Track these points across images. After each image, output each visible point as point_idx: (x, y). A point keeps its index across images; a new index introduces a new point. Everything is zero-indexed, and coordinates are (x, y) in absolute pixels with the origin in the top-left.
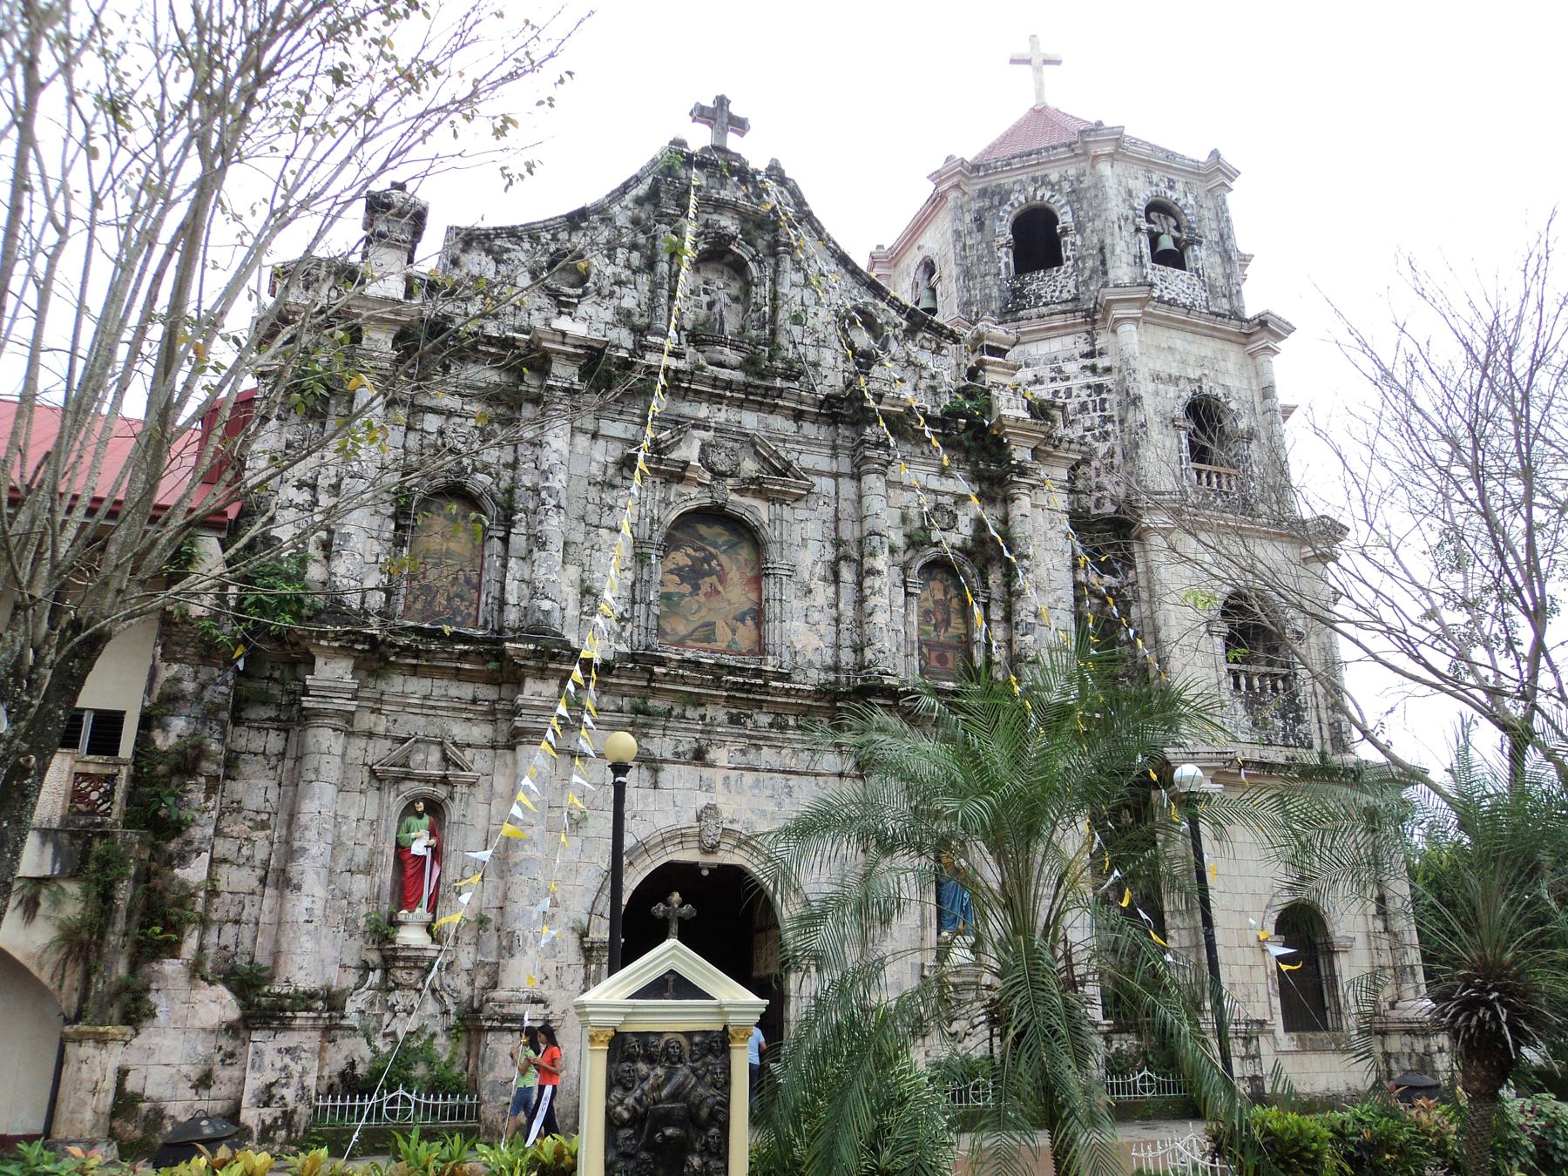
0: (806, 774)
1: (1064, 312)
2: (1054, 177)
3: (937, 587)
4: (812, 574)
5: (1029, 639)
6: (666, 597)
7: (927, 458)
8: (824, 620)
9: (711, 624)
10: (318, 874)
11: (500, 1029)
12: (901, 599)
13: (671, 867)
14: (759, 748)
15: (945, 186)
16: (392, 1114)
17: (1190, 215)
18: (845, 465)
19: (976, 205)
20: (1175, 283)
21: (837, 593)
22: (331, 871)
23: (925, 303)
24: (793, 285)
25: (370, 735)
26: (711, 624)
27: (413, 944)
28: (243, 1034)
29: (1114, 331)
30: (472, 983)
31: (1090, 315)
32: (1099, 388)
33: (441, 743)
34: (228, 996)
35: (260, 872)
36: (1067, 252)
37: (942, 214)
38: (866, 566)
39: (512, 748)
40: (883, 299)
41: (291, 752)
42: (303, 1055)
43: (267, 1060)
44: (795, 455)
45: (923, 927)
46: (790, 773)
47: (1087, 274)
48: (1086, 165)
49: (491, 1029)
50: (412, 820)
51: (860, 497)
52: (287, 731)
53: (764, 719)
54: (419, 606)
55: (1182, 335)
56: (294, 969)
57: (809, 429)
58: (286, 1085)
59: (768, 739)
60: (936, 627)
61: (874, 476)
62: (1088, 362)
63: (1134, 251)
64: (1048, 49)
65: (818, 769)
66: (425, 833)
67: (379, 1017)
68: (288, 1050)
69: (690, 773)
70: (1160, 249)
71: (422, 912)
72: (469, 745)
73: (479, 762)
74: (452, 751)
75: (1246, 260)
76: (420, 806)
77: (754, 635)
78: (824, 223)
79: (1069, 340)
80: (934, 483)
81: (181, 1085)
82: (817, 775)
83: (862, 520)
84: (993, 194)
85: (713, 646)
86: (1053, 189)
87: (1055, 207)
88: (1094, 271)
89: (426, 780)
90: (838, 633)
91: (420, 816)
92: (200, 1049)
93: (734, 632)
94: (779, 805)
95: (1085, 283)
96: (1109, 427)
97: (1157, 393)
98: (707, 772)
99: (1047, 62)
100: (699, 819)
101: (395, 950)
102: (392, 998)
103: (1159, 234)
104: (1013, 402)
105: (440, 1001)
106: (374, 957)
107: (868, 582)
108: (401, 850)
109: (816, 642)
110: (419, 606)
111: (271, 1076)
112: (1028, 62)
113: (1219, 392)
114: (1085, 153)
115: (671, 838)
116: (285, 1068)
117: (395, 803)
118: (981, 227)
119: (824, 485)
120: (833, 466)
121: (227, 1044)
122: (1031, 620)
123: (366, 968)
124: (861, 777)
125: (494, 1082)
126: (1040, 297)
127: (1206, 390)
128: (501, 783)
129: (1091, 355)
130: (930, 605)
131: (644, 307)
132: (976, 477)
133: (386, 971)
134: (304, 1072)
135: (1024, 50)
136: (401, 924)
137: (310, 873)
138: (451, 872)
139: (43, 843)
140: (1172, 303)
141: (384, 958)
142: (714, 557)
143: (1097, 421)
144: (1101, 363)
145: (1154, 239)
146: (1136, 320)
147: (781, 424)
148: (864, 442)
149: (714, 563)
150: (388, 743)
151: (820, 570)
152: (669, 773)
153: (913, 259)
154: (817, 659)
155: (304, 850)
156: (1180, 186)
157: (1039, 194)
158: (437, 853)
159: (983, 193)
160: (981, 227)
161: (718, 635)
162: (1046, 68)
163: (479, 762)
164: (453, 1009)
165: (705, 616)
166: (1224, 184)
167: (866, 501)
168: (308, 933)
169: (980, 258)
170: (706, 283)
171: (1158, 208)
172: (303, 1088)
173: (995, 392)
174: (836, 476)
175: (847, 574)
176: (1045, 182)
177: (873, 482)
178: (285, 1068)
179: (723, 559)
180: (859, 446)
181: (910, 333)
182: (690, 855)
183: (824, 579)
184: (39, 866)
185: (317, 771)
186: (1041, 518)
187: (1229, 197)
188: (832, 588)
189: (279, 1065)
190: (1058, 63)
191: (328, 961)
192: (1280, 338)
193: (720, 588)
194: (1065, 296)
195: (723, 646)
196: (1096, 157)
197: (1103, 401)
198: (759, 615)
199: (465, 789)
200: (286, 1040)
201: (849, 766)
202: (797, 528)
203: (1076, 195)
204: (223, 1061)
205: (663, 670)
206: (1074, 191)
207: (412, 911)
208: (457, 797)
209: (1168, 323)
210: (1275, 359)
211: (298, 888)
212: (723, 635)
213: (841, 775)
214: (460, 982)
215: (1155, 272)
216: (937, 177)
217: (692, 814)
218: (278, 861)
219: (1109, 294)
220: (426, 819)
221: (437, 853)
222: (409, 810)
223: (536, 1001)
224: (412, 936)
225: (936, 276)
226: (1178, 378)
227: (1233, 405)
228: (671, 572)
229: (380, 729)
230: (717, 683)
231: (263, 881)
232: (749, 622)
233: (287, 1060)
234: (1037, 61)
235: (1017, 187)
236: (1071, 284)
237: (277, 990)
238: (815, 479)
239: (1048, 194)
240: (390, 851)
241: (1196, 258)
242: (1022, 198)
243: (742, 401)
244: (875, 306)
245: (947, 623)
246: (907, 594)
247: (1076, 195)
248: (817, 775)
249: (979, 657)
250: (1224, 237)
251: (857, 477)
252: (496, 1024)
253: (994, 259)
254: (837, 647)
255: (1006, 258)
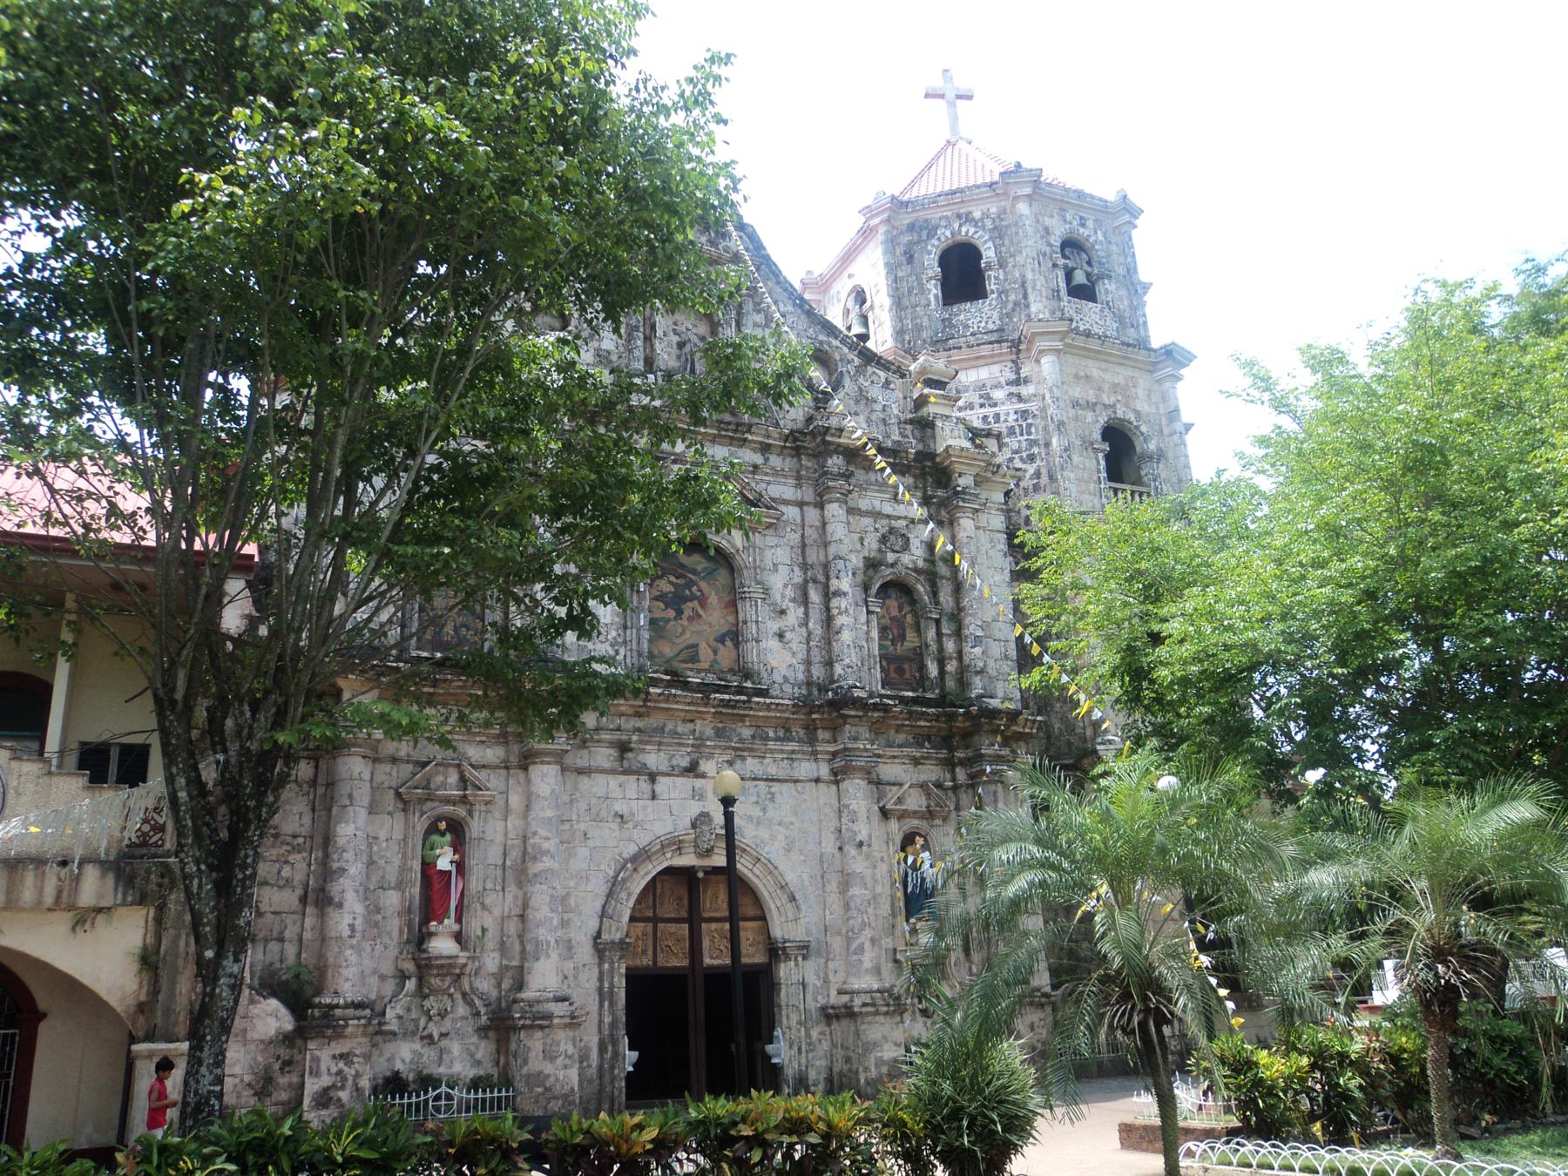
0: (786, 781)
1: (991, 343)
2: (977, 215)
3: (893, 603)
4: (783, 596)
5: (977, 650)
6: (653, 622)
7: (882, 486)
8: (795, 638)
9: (695, 646)
10: (357, 892)
11: (531, 1027)
12: (863, 618)
13: (669, 871)
14: (743, 759)
15: (876, 221)
16: (437, 1109)
17: (1100, 251)
18: (808, 494)
19: (906, 239)
20: (1090, 316)
21: (806, 614)
22: (366, 890)
23: (857, 329)
24: (756, 325)
25: (394, 760)
26: (695, 646)
27: (445, 953)
28: (299, 1042)
29: (1038, 361)
30: (499, 985)
31: (1016, 345)
32: (1024, 414)
33: (458, 766)
34: (283, 1011)
35: (299, 892)
36: (991, 286)
37: (872, 245)
38: (832, 589)
39: (525, 768)
40: (836, 338)
41: (321, 780)
42: (356, 1059)
43: (323, 1067)
44: (763, 485)
45: (894, 915)
46: (773, 780)
47: (1010, 306)
48: (1006, 204)
49: (524, 1027)
50: (435, 838)
51: (824, 524)
52: (317, 760)
53: (746, 733)
54: (428, 636)
55: (1097, 364)
56: (341, 981)
57: (775, 461)
58: (343, 1088)
59: (751, 750)
60: (893, 642)
61: (836, 505)
62: (1014, 389)
63: (1053, 284)
64: (961, 84)
65: (796, 775)
66: (449, 851)
67: (416, 1021)
68: (342, 1056)
69: (685, 784)
70: (1074, 283)
71: (450, 923)
72: (484, 766)
73: (493, 782)
74: (470, 773)
75: (1146, 287)
76: (443, 826)
77: (733, 654)
78: (781, 267)
79: (996, 369)
80: (888, 509)
81: (245, 1093)
82: (796, 781)
83: (826, 545)
84: (921, 229)
85: (697, 666)
86: (976, 226)
87: (978, 243)
88: (1016, 304)
89: (448, 800)
90: (809, 650)
91: (443, 834)
92: (260, 1059)
93: (715, 652)
94: (764, 810)
95: (1008, 315)
96: (1035, 450)
97: (1076, 419)
98: (699, 783)
99: (959, 97)
100: (694, 826)
101: (429, 959)
102: (427, 1004)
103: (1073, 269)
104: (956, 433)
105: (470, 1004)
106: (409, 966)
107: (834, 603)
108: (428, 866)
109: (789, 659)
110: (428, 636)
111: (326, 1081)
112: (942, 96)
113: (1131, 417)
114: (1006, 193)
115: (669, 845)
116: (340, 1072)
117: (420, 824)
118: (910, 260)
119: (792, 512)
120: (798, 495)
121: (284, 1053)
122: (980, 633)
123: (403, 977)
124: (837, 783)
125: (528, 1075)
126: (967, 327)
127: (1120, 414)
128: (515, 800)
129: (1017, 382)
130: (887, 621)
131: (621, 349)
132: (926, 502)
133: (420, 979)
134: (358, 1075)
135: (937, 83)
136: (431, 935)
137: (348, 891)
138: (474, 884)
139: (103, 876)
140: (1088, 334)
141: (419, 967)
142: (694, 583)
143: (1024, 444)
144: (1026, 391)
145: (1069, 275)
146: (1058, 351)
147: (750, 456)
148: (826, 473)
149: (694, 589)
150: (410, 767)
151: (789, 592)
152: (663, 784)
153: (843, 287)
154: (791, 675)
155: (344, 870)
156: (1090, 223)
157: (964, 229)
158: (460, 867)
159: (911, 227)
160: (910, 260)
161: (702, 656)
162: (959, 102)
163: (493, 782)
164: (483, 1010)
165: (689, 638)
166: (1129, 222)
167: (830, 528)
168: (352, 947)
169: (910, 291)
170: (675, 324)
171: (1071, 245)
172: (357, 1089)
173: (939, 423)
174: (801, 504)
175: (815, 596)
176: (968, 218)
177: (834, 510)
178: (340, 1072)
179: (703, 584)
180: (821, 476)
181: (860, 370)
182: (687, 860)
183: (793, 600)
184: (100, 896)
185: (350, 796)
186: (984, 538)
187: (1134, 233)
188: (802, 609)
189: (334, 1070)
190: (970, 98)
191: (367, 971)
192: (1184, 366)
193: (701, 612)
194: (991, 326)
195: (706, 665)
196: (1016, 198)
197: (1030, 426)
198: (735, 636)
199: (483, 808)
200: (339, 1047)
201: (824, 771)
202: (769, 554)
203: (998, 233)
204: (281, 1069)
205: (659, 691)
206: (995, 228)
207: (440, 922)
208: (476, 815)
209: (1087, 353)
210: (1179, 385)
211: (340, 905)
212: (705, 653)
213: (817, 780)
214: (485, 985)
215: (1070, 305)
216: (868, 212)
217: (687, 822)
218: (316, 881)
219: (1028, 329)
220: (448, 837)
221: (460, 867)
222: (432, 829)
223: (564, 999)
224: (442, 945)
225: (868, 304)
226: (1095, 405)
227: (1144, 428)
228: (656, 599)
229: (402, 753)
230: (706, 701)
231: (303, 900)
232: (729, 643)
233: (341, 1065)
234: (950, 95)
235: (943, 223)
236: (996, 315)
237: (328, 1001)
238: (783, 508)
239: (972, 230)
240: (417, 866)
241: (1107, 292)
242: (948, 233)
243: (715, 436)
244: (829, 344)
245: (903, 637)
246: (869, 612)
247: (998, 233)
248: (796, 781)
249: (933, 670)
250: (1131, 270)
251: (821, 506)
252: (528, 1022)
253: (923, 291)
254: (808, 663)
255: (934, 290)
